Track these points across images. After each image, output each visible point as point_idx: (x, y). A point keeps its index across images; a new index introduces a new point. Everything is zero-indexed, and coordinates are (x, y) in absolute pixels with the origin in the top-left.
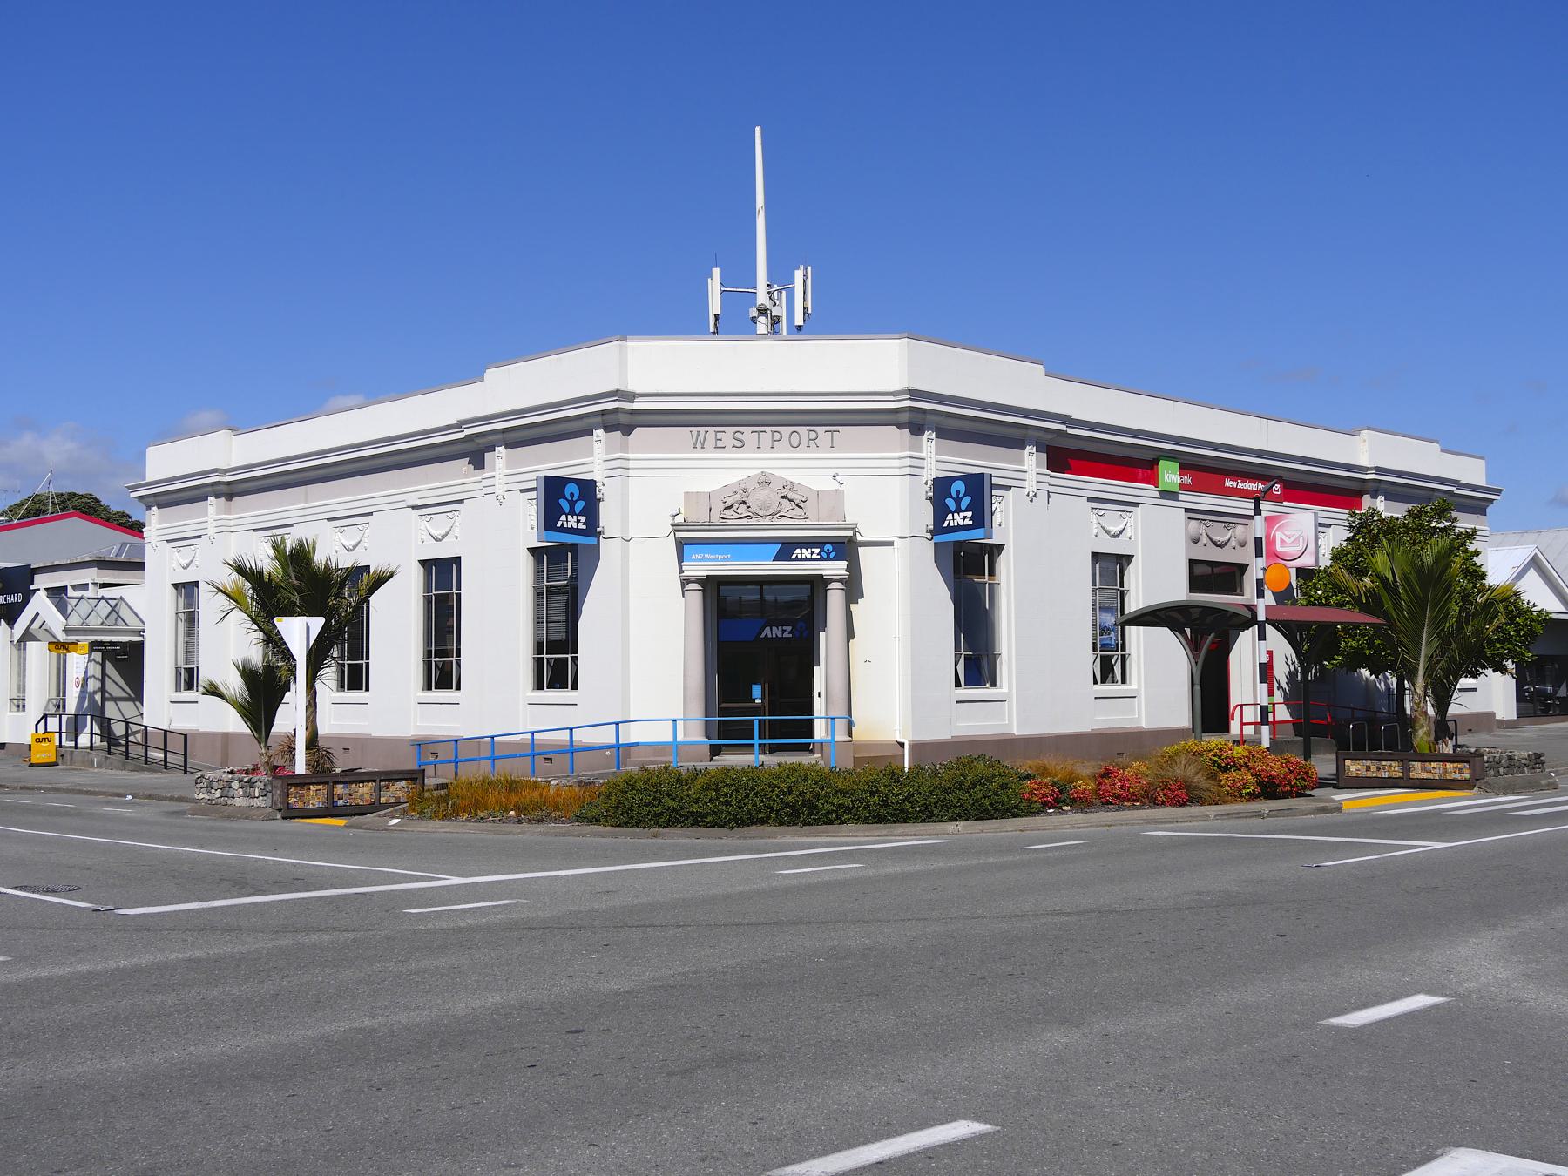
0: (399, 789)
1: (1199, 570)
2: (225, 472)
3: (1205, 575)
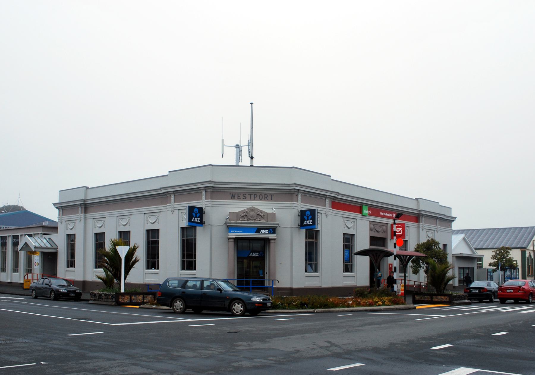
0: (149, 297)
1: (346, 236)
2: (215, 183)
3: (373, 240)
